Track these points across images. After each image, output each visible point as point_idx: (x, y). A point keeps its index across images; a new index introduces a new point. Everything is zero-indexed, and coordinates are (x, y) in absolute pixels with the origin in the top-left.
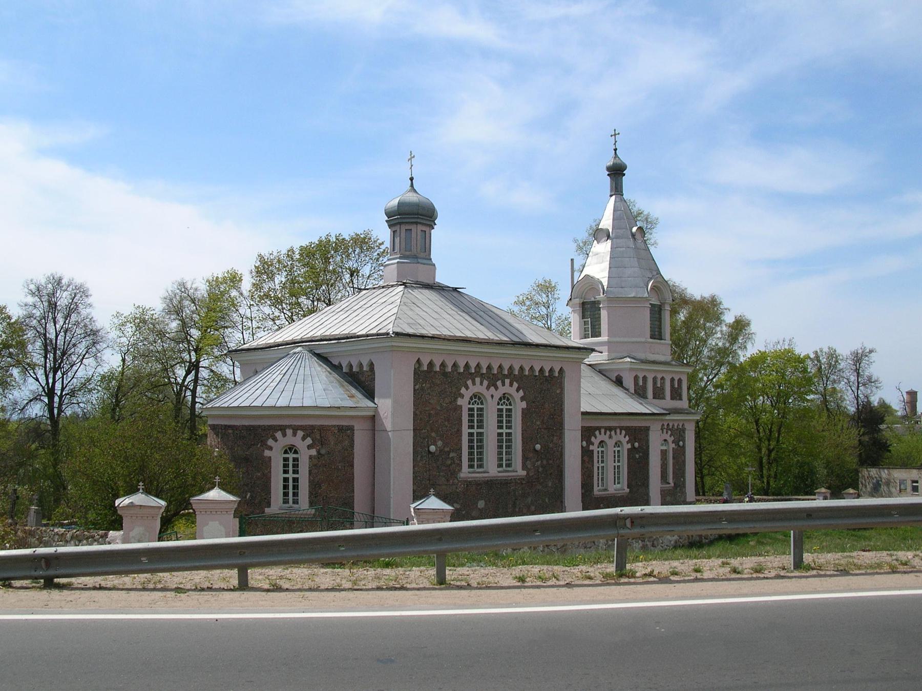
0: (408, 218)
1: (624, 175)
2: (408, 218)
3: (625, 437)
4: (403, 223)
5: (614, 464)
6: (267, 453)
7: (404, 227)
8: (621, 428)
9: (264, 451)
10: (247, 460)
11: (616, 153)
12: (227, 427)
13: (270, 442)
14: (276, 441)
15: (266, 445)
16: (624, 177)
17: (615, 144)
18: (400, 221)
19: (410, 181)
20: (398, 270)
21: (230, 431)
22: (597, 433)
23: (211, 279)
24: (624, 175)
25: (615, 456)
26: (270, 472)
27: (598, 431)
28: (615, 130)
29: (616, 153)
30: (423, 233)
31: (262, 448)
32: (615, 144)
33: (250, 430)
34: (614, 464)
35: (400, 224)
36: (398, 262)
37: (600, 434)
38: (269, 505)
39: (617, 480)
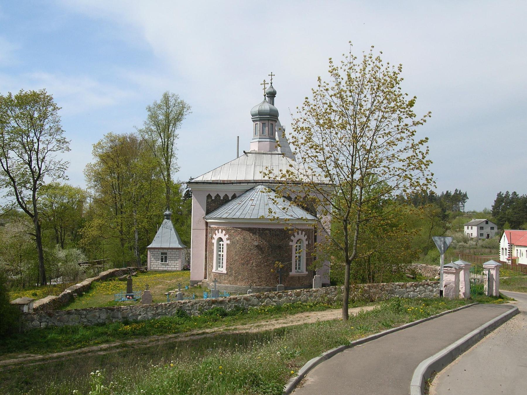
0: (273, 118)
1: (275, 96)
2: (273, 118)
3: (305, 236)
4: (270, 120)
5: (223, 253)
6: (291, 243)
7: (270, 122)
8: (302, 230)
9: (289, 242)
10: (280, 247)
11: (271, 85)
12: (264, 229)
13: (292, 238)
14: (295, 237)
15: (290, 239)
16: (275, 98)
17: (271, 80)
18: (270, 119)
19: (264, 96)
20: (270, 146)
21: (267, 232)
22: (217, 232)
23: (152, 106)
24: (275, 96)
25: (223, 249)
26: (292, 253)
27: (217, 231)
28: (272, 73)
29: (271, 85)
30: (272, 125)
31: (288, 241)
32: (271, 80)
33: (282, 231)
34: (223, 253)
35: (269, 120)
36: (270, 141)
37: (218, 233)
38: (291, 271)
39: (219, 265)
